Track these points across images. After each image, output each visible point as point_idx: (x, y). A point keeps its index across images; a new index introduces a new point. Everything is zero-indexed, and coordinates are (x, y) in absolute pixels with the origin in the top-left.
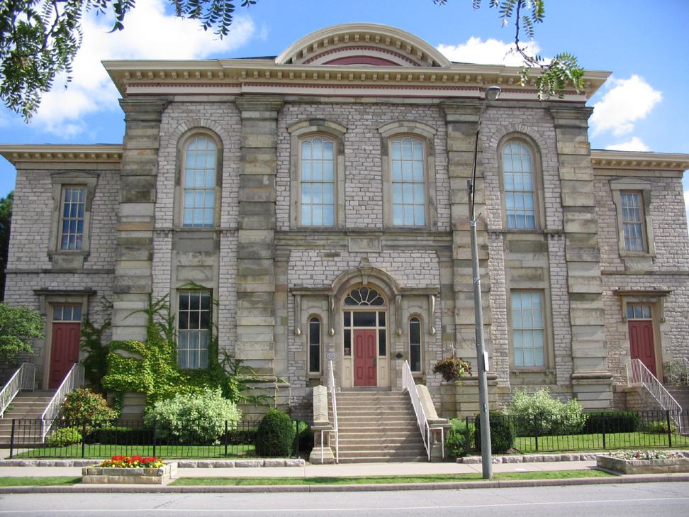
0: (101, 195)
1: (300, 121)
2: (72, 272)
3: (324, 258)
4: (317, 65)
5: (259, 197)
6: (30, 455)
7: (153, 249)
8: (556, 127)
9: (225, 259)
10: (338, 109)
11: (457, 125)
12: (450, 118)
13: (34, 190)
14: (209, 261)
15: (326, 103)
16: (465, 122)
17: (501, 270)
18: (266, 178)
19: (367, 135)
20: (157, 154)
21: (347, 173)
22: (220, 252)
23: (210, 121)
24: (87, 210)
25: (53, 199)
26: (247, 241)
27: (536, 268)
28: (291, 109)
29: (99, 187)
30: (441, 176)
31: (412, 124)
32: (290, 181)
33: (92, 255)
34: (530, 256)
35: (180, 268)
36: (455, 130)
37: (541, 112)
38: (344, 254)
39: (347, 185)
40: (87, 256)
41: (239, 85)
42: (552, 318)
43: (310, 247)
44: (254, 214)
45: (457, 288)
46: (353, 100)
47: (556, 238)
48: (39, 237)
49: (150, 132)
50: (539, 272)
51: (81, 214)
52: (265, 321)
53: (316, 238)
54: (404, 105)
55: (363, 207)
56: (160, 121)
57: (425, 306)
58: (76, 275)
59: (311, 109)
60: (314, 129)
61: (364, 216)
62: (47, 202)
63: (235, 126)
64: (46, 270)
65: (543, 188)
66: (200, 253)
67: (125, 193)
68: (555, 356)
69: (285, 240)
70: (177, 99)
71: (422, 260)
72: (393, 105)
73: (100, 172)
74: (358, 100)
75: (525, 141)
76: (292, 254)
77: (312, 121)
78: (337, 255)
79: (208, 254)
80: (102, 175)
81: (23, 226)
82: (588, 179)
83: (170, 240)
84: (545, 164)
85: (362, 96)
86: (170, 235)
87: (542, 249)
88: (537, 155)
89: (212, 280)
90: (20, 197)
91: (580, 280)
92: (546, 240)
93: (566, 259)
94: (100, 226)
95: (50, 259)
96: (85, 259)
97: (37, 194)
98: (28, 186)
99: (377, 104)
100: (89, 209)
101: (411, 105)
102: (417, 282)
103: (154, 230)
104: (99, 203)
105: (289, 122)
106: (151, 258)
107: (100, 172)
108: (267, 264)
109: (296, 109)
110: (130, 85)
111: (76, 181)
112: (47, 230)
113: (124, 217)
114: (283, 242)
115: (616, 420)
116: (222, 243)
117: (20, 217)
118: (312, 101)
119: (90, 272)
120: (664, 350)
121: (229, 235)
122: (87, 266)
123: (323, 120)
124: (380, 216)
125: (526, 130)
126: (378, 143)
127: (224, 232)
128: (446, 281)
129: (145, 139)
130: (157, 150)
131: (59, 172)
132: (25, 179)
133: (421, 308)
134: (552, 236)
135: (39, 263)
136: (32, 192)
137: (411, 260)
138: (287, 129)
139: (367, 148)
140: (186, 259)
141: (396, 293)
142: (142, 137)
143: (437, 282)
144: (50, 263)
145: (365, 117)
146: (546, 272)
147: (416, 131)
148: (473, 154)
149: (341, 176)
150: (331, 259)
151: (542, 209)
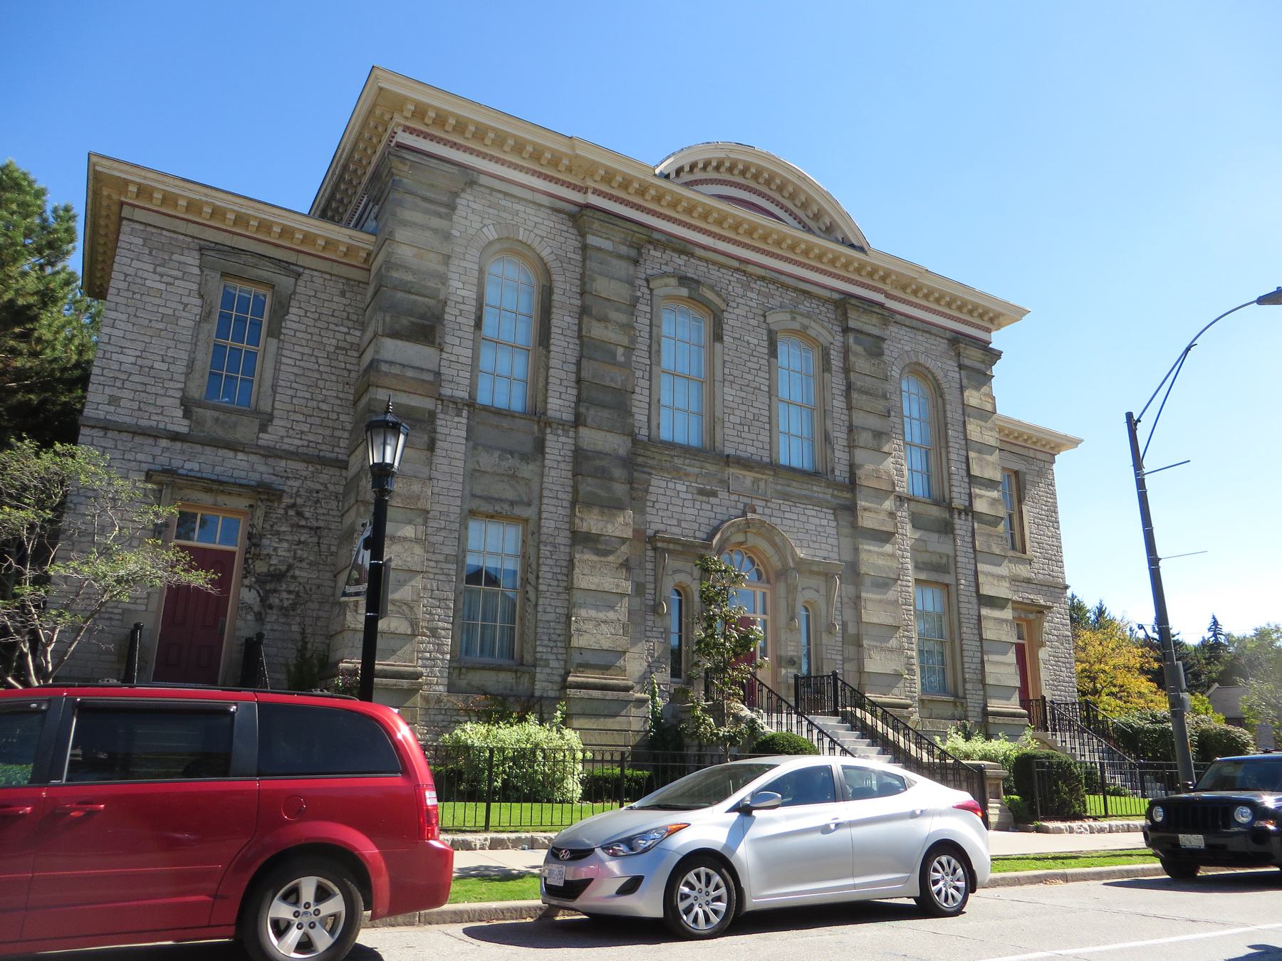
0: (302, 313)
1: (665, 274)
2: (234, 447)
3: (696, 497)
4: (701, 197)
5: (612, 380)
6: (603, 894)
7: (435, 432)
8: (961, 367)
9: (553, 473)
10: (715, 273)
11: (860, 336)
12: (852, 324)
13: (159, 269)
14: (528, 470)
15: (700, 259)
16: (869, 335)
17: (905, 550)
18: (620, 351)
19: (752, 322)
20: (447, 265)
21: (727, 371)
22: (544, 459)
23: (532, 235)
24: (270, 334)
25: (201, 296)
26: (591, 447)
27: (941, 555)
28: (652, 252)
29: (297, 297)
30: (839, 403)
31: (806, 321)
32: (651, 365)
33: (276, 422)
34: (935, 536)
35: (477, 474)
36: (858, 342)
37: (943, 344)
38: (723, 494)
39: (726, 389)
40: (265, 421)
41: (583, 190)
42: (960, 627)
43: (678, 474)
44: (603, 406)
45: (863, 570)
46: (736, 264)
47: (963, 516)
48: (165, 367)
49: (435, 222)
50: (944, 561)
51: (255, 340)
52: (618, 585)
53: (687, 461)
54: (796, 289)
55: (746, 428)
56: (453, 208)
57: (823, 591)
58: (240, 456)
59: (680, 260)
60: (684, 292)
61: (747, 442)
62: (185, 300)
63: (573, 256)
64: (177, 433)
65: (948, 447)
66: (512, 453)
67: (388, 319)
68: (964, 681)
69: (644, 456)
70: (483, 180)
71: (817, 521)
72: (783, 285)
73: (301, 270)
74: (743, 267)
75: (924, 377)
76: (654, 482)
77: (683, 280)
78: (714, 494)
79: (525, 458)
80: (305, 277)
81: (128, 336)
82: (994, 444)
83: (464, 421)
84: (949, 414)
85: (747, 262)
86: (465, 413)
87: (946, 529)
88: (940, 401)
89: (529, 504)
90: (126, 275)
91: (990, 578)
92: (952, 517)
93: (974, 547)
94: (296, 370)
95: (187, 414)
96: (263, 428)
97: (165, 279)
98: (146, 258)
99: (763, 278)
100: (275, 332)
101: (804, 292)
102: (811, 552)
103: (440, 398)
104: (295, 326)
105: (649, 272)
106: (431, 447)
107: (301, 270)
108: (620, 489)
109: (659, 254)
110: (406, 129)
111: (254, 273)
112: (185, 356)
113: (386, 362)
114: (640, 460)
115: (502, 718)
116: (548, 444)
117: (124, 317)
118: (683, 248)
119: (270, 453)
120: (1043, 683)
121: (560, 432)
122: (266, 439)
123: (698, 282)
124: (767, 447)
125: (930, 363)
126: (765, 338)
127: (554, 426)
128: (847, 557)
129: (428, 234)
130: (447, 258)
131: (219, 248)
132: (141, 242)
133: (817, 591)
134: (960, 514)
135: (160, 418)
136: (155, 272)
137: (804, 518)
138: (648, 281)
139: (752, 341)
140: (488, 461)
141: (792, 564)
142: (424, 227)
143: (835, 556)
144: (186, 422)
145: (749, 294)
146: (951, 560)
147: (812, 333)
148: (677, 380)
149: (719, 376)
150: (705, 498)
151: (945, 474)
